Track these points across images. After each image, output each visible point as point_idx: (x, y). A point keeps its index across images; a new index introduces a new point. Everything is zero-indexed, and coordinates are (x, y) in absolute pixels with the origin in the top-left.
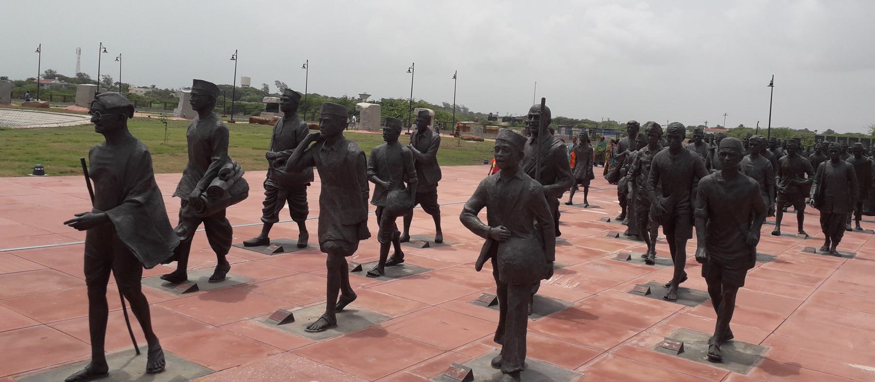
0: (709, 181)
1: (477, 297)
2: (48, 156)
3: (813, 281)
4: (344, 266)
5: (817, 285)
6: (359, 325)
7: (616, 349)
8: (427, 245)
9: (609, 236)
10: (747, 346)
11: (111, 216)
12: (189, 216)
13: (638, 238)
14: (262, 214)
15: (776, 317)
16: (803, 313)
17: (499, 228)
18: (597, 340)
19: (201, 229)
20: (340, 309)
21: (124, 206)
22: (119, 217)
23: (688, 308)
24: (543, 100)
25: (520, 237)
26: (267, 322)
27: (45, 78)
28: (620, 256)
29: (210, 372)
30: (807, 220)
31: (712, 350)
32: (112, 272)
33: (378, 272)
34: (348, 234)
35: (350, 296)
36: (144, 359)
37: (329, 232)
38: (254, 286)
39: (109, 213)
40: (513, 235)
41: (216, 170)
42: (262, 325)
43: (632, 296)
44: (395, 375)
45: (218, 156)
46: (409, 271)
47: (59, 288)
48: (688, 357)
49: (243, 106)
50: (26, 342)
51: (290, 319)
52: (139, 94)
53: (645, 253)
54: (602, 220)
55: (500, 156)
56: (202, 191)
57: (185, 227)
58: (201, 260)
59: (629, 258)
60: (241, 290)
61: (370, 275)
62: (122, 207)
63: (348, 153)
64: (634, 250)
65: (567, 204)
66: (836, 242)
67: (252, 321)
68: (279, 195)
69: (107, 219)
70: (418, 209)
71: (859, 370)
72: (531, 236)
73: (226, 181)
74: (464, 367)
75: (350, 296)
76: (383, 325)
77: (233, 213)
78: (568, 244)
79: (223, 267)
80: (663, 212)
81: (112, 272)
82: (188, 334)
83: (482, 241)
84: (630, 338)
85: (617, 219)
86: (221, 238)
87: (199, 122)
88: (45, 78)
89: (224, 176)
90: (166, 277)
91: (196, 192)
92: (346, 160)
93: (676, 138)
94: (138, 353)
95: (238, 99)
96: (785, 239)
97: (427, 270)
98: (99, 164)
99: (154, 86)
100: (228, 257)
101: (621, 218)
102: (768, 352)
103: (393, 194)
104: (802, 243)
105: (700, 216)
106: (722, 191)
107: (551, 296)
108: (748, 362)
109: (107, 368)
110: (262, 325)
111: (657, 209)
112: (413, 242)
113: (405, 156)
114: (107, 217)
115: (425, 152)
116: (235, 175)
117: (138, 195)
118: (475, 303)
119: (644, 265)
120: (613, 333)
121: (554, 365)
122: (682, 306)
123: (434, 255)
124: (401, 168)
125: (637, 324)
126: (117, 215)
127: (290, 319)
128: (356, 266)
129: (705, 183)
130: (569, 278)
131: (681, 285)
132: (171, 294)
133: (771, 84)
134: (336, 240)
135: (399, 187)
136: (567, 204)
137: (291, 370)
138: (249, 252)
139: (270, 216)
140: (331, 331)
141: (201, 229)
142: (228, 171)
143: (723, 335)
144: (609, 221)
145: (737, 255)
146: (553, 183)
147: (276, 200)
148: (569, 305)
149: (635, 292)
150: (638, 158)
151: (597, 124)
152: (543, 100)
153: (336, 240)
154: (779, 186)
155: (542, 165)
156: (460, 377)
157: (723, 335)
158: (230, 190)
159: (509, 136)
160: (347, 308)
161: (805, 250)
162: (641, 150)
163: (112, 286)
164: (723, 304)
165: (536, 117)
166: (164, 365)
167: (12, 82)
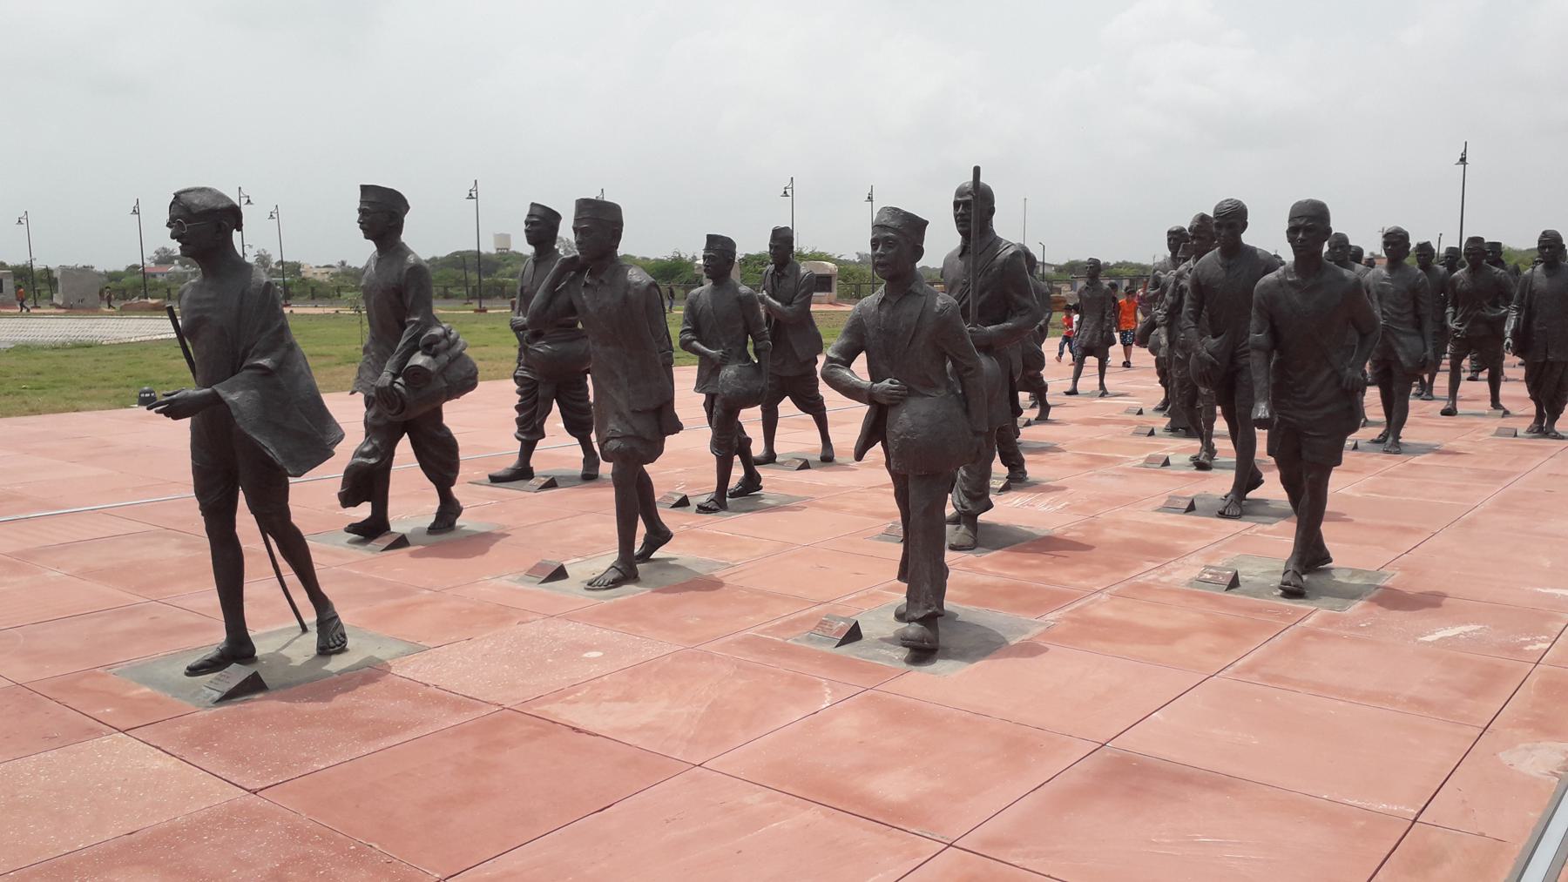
0: (1273, 282)
1: (883, 530)
2: (163, 378)
3: (1499, 477)
4: (645, 485)
5: (1506, 482)
6: (676, 578)
7: (1115, 588)
8: (805, 465)
9: (1136, 433)
10: (1355, 573)
11: (222, 392)
12: (379, 422)
13: (1189, 434)
14: (515, 428)
15: (1419, 531)
16: (1470, 523)
17: (886, 383)
18: (1085, 576)
19: (404, 447)
20: (645, 556)
21: (243, 375)
22: (235, 396)
23: (1260, 527)
24: (977, 171)
25: (924, 396)
26: (521, 580)
27: (157, 263)
28: (1150, 461)
29: (423, 650)
30: (1504, 390)
31: (1288, 577)
32: (241, 493)
33: (719, 503)
34: (643, 426)
35: (659, 535)
36: (313, 637)
37: (612, 425)
38: (504, 535)
39: (220, 389)
40: (911, 392)
41: (416, 338)
42: (512, 585)
43: (1160, 515)
44: (730, 638)
45: (416, 315)
46: (770, 502)
47: (180, 553)
48: (1246, 593)
49: (503, 285)
50: (126, 624)
51: (560, 574)
52: (319, 278)
53: (1196, 453)
54: (1127, 411)
55: (880, 256)
56: (395, 376)
57: (376, 442)
58: (411, 497)
59: (1166, 463)
60: (481, 542)
61: (703, 509)
62: (238, 377)
63: (628, 285)
64: (1178, 451)
65: (1068, 393)
66: (1556, 414)
67: (495, 579)
68: (540, 392)
69: (216, 399)
70: (787, 407)
71: (1554, 595)
72: (943, 392)
73: (434, 356)
74: (843, 619)
75: (659, 535)
76: (718, 575)
77: (456, 415)
78: (1060, 450)
79: (449, 510)
80: (1213, 364)
81: (241, 493)
82: (392, 602)
83: (863, 409)
84: (1147, 572)
85: (1157, 410)
86: (440, 460)
87: (379, 260)
88: (157, 263)
89: (428, 349)
90: (354, 528)
91: (385, 378)
92: (626, 298)
93: (1231, 226)
94: (304, 629)
95: (488, 274)
96: (1464, 420)
97: (801, 499)
98: (196, 311)
99: (343, 263)
100: (455, 490)
101: (1162, 408)
102: (1393, 579)
103: (729, 372)
104: (1498, 422)
105: (1257, 348)
106: (1296, 297)
107: (1014, 523)
108: (1351, 594)
109: (254, 650)
110: (512, 585)
111: (1200, 359)
112: (782, 464)
113: (747, 303)
114: (215, 394)
115: (789, 304)
116: (448, 348)
117: (262, 357)
118: (879, 539)
119: (1193, 470)
120: (1115, 566)
121: (1004, 614)
122: (1249, 524)
123: (819, 478)
124: (741, 325)
125: (1162, 552)
126: (232, 391)
127: (560, 574)
128: (678, 498)
129: (1265, 287)
130: (1050, 497)
131: (1251, 495)
132: (369, 554)
133: (1463, 160)
134: (623, 437)
135: (739, 358)
136: (1068, 393)
137: (556, 640)
138: (500, 490)
139: (530, 430)
140: (629, 589)
141: (404, 447)
142: (436, 339)
143: (1311, 555)
144: (1140, 413)
145: (1329, 409)
146: (1004, 321)
147: (535, 402)
148: (1045, 534)
149: (1166, 508)
150: (1176, 283)
151: (1144, 268)
152: (977, 171)
153: (623, 437)
154: (1453, 326)
155: (981, 293)
156: (838, 634)
157: (1311, 555)
158: (443, 370)
159: (894, 218)
160: (654, 556)
161: (1497, 434)
162: (1182, 268)
163: (246, 523)
164: (1306, 499)
165: (966, 204)
166: (344, 642)
167: (100, 275)
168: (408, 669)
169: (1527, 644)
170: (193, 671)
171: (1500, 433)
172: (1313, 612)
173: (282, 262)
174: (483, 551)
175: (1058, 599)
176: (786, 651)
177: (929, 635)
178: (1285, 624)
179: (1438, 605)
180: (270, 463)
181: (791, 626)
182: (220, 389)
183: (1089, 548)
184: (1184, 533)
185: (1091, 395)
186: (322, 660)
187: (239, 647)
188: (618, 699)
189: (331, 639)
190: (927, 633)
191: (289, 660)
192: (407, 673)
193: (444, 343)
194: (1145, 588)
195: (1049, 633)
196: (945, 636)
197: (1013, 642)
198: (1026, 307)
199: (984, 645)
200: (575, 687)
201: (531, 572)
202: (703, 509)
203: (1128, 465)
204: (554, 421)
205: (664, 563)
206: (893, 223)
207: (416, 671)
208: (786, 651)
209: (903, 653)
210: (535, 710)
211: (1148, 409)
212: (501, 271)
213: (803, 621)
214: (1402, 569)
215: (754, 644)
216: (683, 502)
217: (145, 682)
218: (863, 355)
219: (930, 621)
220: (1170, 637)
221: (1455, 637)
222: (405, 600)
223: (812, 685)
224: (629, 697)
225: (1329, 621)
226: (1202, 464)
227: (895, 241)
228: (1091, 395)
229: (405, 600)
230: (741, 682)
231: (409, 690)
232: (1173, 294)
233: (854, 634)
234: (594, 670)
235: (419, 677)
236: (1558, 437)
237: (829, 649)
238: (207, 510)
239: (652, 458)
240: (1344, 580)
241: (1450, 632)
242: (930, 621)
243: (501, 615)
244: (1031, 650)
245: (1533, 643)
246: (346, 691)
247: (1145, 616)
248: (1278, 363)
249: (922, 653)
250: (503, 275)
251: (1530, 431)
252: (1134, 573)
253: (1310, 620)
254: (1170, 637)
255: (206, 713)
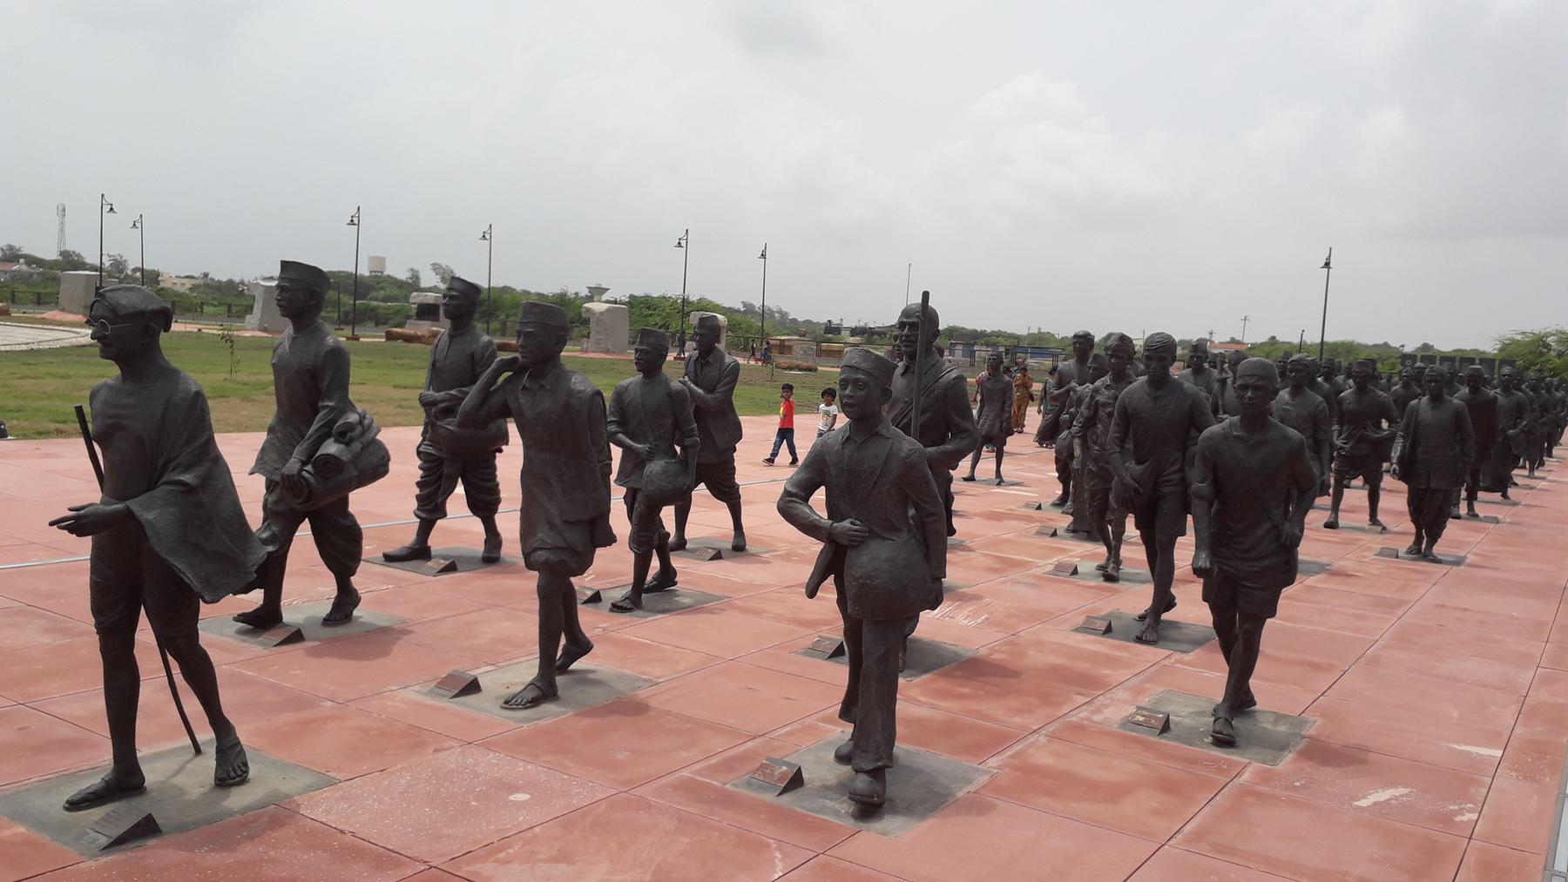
1: (809, 642)
3: (1392, 606)
6: (597, 696)
7: (1051, 728)
8: (718, 556)
9: (1040, 533)
10: (1279, 718)
12: (281, 508)
13: (1090, 537)
14: (414, 504)
15: (1329, 668)
16: (1375, 661)
17: (846, 524)
19: (305, 531)
20: (563, 669)
21: (161, 491)
22: (152, 512)
23: (1177, 656)
24: (926, 295)
25: (885, 539)
26: (430, 693)
28: (1059, 568)
29: (332, 783)
30: (1384, 502)
33: (632, 603)
34: (575, 537)
35: (581, 646)
36: (209, 761)
37: (541, 535)
38: (405, 632)
39: (134, 505)
40: (872, 535)
41: (329, 424)
43: (1079, 636)
44: (664, 781)
45: (331, 399)
46: (686, 601)
47: (46, 640)
48: (1178, 738)
51: (473, 687)
53: (1102, 562)
54: (1027, 506)
56: (304, 463)
57: (275, 529)
58: (307, 586)
59: (1075, 572)
60: (382, 638)
61: (617, 608)
63: (571, 393)
66: (1434, 537)
67: (404, 692)
69: (129, 514)
70: (701, 492)
73: (347, 444)
75: (581, 646)
76: (642, 694)
77: (361, 502)
79: (346, 600)
80: (1136, 490)
82: (288, 717)
83: (816, 547)
84: (1077, 708)
85: (1054, 505)
86: (341, 547)
89: (343, 436)
91: (293, 465)
92: (567, 407)
93: (1161, 359)
97: (718, 598)
98: (110, 417)
99: (206, 275)
101: (1061, 502)
103: (655, 467)
104: (1376, 542)
107: (938, 639)
109: (143, 780)
112: (693, 551)
113: (676, 399)
118: (805, 654)
119: (1100, 582)
120: (1046, 699)
121: (944, 757)
123: (731, 572)
124: (670, 421)
125: (1090, 683)
126: (148, 509)
127: (473, 687)
128: (589, 593)
129: (1209, 438)
130: (968, 609)
131: (1165, 616)
132: (256, 649)
133: (1327, 265)
137: (477, 775)
138: (395, 571)
139: (431, 508)
141: (305, 531)
142: (350, 427)
143: (1239, 699)
144: (1039, 508)
145: (1266, 563)
148: (970, 654)
149: (1085, 629)
150: (1092, 397)
151: (1018, 338)
152: (926, 295)
154: (1339, 443)
155: (923, 413)
156: (780, 779)
157: (1239, 699)
158: (356, 458)
159: (865, 360)
160: (574, 666)
162: (1098, 383)
163: (145, 635)
164: (1239, 647)
166: (246, 772)
168: (322, 809)
169: (1457, 813)
170: (74, 805)
171: (1384, 553)
172: (1248, 767)
173: (142, 270)
174: (383, 652)
175: (995, 741)
176: (727, 800)
177: (876, 779)
178: (1223, 780)
179: (1364, 762)
180: (188, 588)
181: (728, 766)
182: (134, 505)
183: (1016, 674)
184: (1109, 661)
185: (987, 482)
186: (220, 793)
187: (126, 779)
188: (554, 860)
189: (232, 767)
190: (878, 787)
191: (181, 791)
192: (318, 814)
193: (359, 429)
194: (1078, 728)
195: (992, 786)
196: (895, 787)
197: (960, 794)
198: (967, 430)
199: (932, 799)
200: (505, 841)
201: (443, 684)
202: (617, 608)
203: (1039, 571)
204: (458, 498)
205: (584, 678)
206: (864, 365)
207: (328, 812)
208: (727, 800)
209: (846, 807)
210: (465, 870)
211: (1047, 502)
212: (374, 294)
213: (742, 759)
214: (1323, 716)
215: (690, 789)
216: (596, 598)
217: (20, 817)
218: (823, 488)
219: (877, 774)
220: (1115, 793)
221: (1388, 802)
222: (305, 714)
223: (760, 847)
224: (564, 857)
225: (1265, 778)
226: (1110, 574)
227: (866, 384)
228: (987, 482)
229: (305, 714)
230: (685, 840)
231: (323, 838)
232: (1088, 408)
233: (796, 781)
234: (523, 818)
235: (331, 820)
236: (1436, 561)
237: (770, 797)
238: (102, 629)
239: (580, 571)
240: (1269, 726)
241: (1382, 796)
242: (877, 774)
243: (413, 739)
244: (977, 806)
245: (1460, 812)
246: (251, 838)
247: (1086, 765)
248: (1218, 512)
249: (869, 808)
250: (376, 299)
251: (1410, 552)
252: (1066, 709)
253: (1246, 776)
254: (1115, 793)
255: (92, 864)
